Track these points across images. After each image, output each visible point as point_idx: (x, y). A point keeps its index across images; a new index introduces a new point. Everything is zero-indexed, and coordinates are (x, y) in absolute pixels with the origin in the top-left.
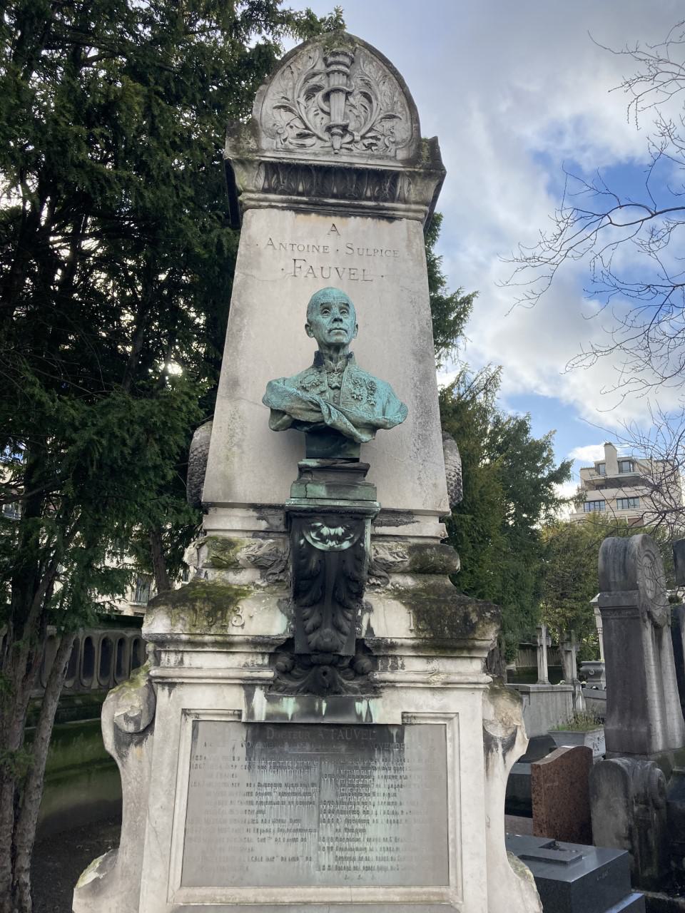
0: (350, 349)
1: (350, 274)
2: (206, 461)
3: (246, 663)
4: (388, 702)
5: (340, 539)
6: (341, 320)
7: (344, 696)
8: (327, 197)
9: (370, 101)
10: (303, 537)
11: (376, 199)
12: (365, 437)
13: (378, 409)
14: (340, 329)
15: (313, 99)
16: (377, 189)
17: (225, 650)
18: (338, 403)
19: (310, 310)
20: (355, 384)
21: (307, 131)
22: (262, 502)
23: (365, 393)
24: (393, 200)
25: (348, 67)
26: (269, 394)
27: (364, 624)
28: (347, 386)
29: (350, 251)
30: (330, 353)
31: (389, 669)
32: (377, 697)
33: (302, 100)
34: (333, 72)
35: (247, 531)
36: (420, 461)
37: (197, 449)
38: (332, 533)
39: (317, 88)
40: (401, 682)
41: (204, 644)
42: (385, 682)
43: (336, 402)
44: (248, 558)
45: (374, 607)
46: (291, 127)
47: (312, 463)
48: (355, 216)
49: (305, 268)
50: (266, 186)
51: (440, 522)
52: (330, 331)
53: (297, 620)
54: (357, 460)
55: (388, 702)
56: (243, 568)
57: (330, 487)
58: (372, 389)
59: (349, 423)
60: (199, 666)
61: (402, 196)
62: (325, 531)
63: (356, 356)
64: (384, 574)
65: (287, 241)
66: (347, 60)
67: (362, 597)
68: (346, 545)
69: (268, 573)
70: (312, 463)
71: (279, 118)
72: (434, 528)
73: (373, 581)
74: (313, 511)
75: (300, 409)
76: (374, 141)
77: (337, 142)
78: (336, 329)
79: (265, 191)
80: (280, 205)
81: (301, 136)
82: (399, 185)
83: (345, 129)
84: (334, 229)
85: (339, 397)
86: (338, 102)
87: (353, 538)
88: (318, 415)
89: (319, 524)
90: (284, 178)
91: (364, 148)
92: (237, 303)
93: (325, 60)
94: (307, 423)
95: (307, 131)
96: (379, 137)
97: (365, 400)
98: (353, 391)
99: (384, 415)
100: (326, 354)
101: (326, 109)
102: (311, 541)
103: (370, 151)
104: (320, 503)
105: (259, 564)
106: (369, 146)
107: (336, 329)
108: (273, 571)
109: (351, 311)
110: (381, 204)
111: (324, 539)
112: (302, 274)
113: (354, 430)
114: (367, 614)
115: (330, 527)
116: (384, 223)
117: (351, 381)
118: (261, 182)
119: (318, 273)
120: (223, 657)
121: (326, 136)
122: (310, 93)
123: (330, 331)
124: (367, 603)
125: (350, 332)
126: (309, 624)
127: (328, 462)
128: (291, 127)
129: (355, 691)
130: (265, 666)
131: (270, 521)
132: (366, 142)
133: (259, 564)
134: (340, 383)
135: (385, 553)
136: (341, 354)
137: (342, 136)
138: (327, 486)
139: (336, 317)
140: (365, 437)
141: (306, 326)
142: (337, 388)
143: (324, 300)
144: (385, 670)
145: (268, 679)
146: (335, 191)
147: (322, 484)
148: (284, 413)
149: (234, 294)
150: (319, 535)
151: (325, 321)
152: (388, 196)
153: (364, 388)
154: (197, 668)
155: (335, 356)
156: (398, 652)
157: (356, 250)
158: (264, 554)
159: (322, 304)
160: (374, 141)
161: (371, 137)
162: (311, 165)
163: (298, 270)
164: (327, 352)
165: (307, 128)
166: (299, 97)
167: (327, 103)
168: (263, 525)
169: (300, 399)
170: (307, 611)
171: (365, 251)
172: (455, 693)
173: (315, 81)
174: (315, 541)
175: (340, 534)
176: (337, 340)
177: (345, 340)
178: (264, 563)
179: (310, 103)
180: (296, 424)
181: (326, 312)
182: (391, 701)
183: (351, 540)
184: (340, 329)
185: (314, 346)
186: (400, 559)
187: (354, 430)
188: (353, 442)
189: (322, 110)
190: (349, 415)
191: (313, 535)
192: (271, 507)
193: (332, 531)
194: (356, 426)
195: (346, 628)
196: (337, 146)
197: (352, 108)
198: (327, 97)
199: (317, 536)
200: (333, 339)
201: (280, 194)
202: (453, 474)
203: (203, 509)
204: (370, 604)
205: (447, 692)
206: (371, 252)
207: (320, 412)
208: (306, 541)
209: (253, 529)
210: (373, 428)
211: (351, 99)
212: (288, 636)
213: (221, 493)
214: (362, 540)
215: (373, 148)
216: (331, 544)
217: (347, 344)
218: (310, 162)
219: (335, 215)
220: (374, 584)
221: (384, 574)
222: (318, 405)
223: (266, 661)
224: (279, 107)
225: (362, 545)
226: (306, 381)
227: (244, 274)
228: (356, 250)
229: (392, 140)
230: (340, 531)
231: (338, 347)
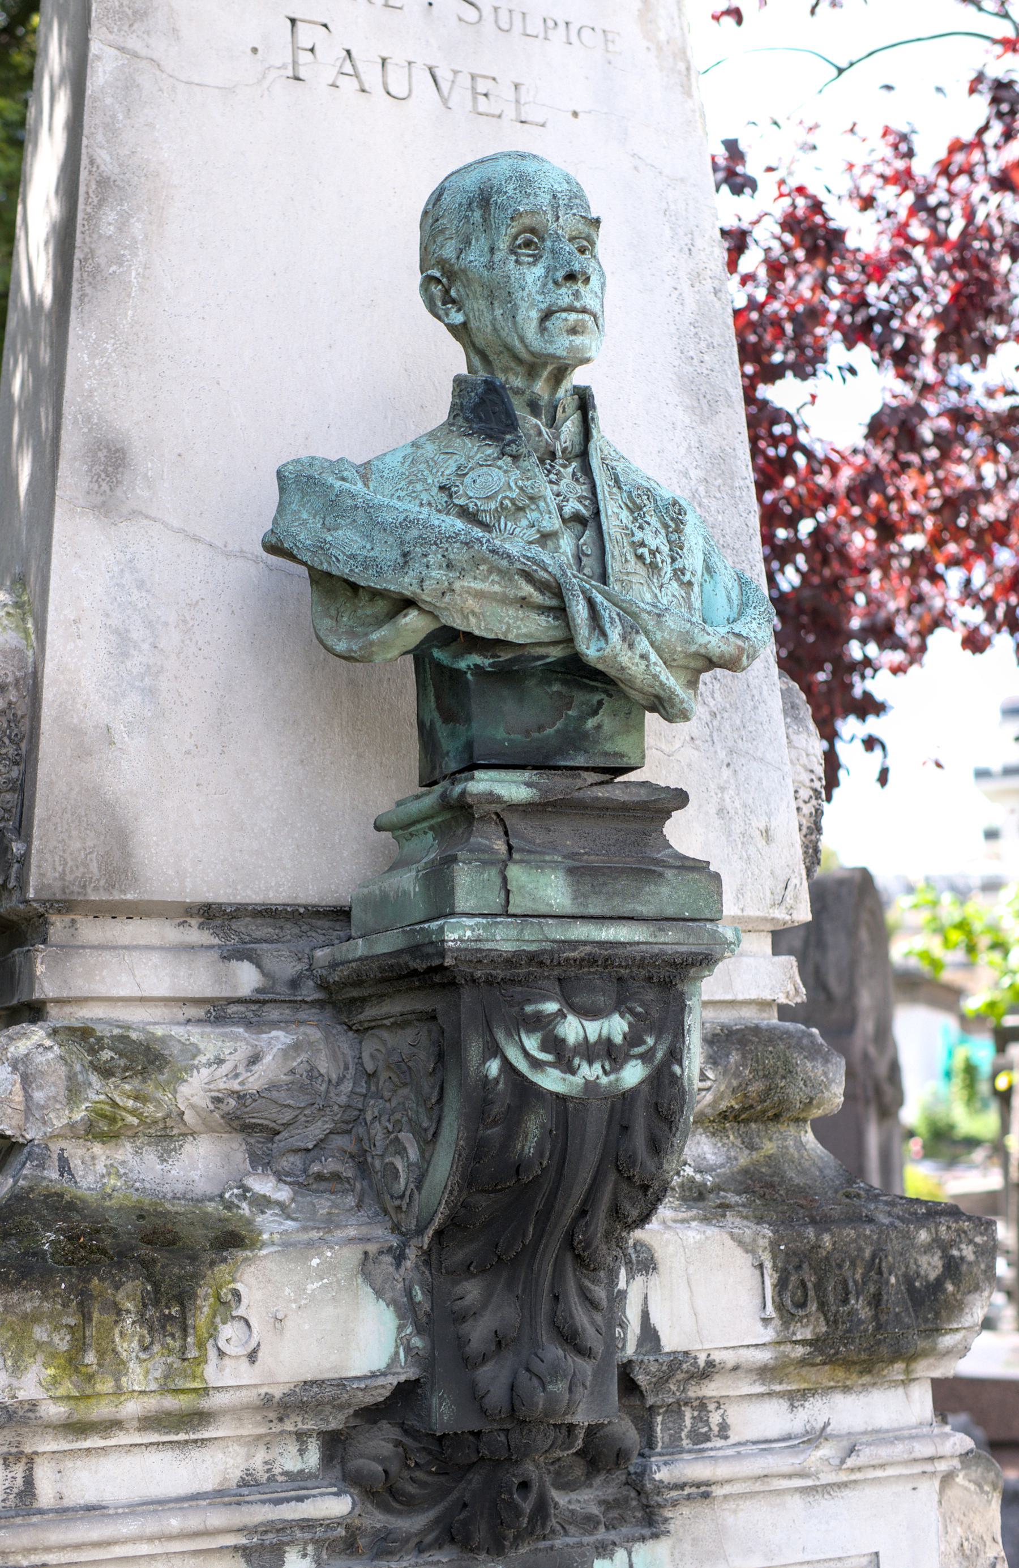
1: (475, 93)
3: (248, 1472)
4: (687, 1547)
5: (610, 1053)
7: (558, 1543)
10: (495, 1050)
17: (182, 1437)
22: (239, 899)
27: (632, 1314)
30: (509, 398)
31: (686, 1443)
32: (655, 1536)
35: (185, 1001)
36: (722, 754)
38: (592, 1038)
40: (728, 1481)
41: (114, 1425)
42: (682, 1486)
44: (217, 1100)
45: (659, 1255)
49: (330, 54)
51: (776, 952)
52: (547, 315)
53: (434, 1324)
55: (687, 1547)
57: (579, 873)
60: (91, 1497)
74: (534, 959)
87: (652, 1050)
89: (551, 1007)
92: (103, 156)
98: (639, 536)
102: (522, 1065)
104: (557, 932)
111: (563, 1055)
114: (639, 1279)
119: (372, 76)
120: (167, 1456)
126: (478, 1333)
127: (559, 784)
129: (589, 1523)
130: (311, 1476)
131: (269, 963)
138: (571, 871)
144: (674, 1448)
145: (339, 1521)
147: (555, 866)
150: (554, 1044)
154: (90, 1508)
156: (710, 1389)
158: (273, 1086)
163: (304, 57)
168: (246, 978)
170: (472, 1291)
172: (870, 1493)
175: (618, 1039)
178: (267, 1115)
182: (695, 1541)
183: (646, 1058)
191: (531, 1043)
192: (267, 913)
193: (594, 1029)
195: (592, 1338)
199: (544, 1048)
204: (649, 1249)
205: (847, 1493)
206: (535, 26)
208: (508, 1066)
209: (209, 993)
212: (407, 1373)
213: (94, 867)
214: (675, 1055)
216: (590, 1072)
223: (313, 1458)
225: (677, 1069)
227: (122, 49)
230: (616, 1027)
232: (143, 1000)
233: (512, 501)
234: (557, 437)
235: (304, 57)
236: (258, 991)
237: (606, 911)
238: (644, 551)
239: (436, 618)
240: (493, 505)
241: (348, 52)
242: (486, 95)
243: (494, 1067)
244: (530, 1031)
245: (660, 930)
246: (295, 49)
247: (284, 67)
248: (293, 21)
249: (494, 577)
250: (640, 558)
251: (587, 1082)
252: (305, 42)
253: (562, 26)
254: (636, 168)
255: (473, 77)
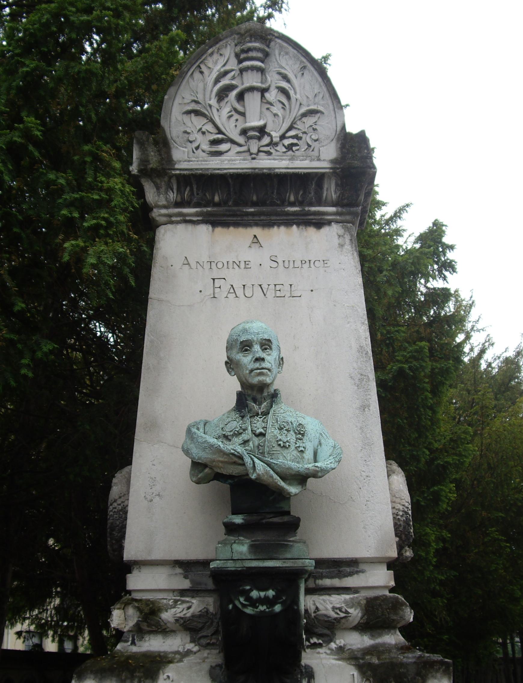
0: (274, 387)
1: (276, 291)
2: (126, 513)
5: (265, 601)
6: (263, 360)
8: (246, 205)
9: (288, 97)
10: (232, 602)
11: (301, 204)
12: (293, 490)
13: (308, 454)
14: (263, 368)
15: (226, 100)
16: (301, 193)
18: (263, 453)
19: (229, 348)
20: (281, 429)
21: (220, 136)
23: (292, 437)
24: (320, 203)
25: (262, 62)
26: (189, 442)
28: (272, 432)
29: (274, 265)
30: (254, 397)
33: (213, 102)
34: (247, 69)
35: (173, 591)
37: (115, 501)
39: (229, 88)
43: (261, 452)
46: (204, 133)
47: (238, 520)
48: (279, 225)
49: (226, 287)
50: (179, 199)
54: (288, 513)
56: (173, 631)
58: (301, 433)
59: (275, 476)
61: (329, 198)
62: (255, 594)
63: (283, 394)
64: (326, 631)
65: (205, 259)
66: (260, 55)
67: (300, 661)
68: (278, 608)
69: (200, 635)
70: (238, 520)
71: (189, 124)
72: (381, 578)
73: (314, 640)
75: (222, 462)
76: (295, 141)
77: (254, 146)
78: (258, 369)
79: (177, 205)
80: (195, 219)
81: (215, 142)
82: (326, 186)
83: (262, 131)
84: (255, 240)
85: (264, 446)
86: (253, 101)
88: (241, 468)
89: (248, 588)
90: (198, 189)
91: (285, 150)
93: (237, 56)
94: (231, 477)
95: (220, 136)
96: (300, 135)
97: (293, 448)
98: (280, 437)
99: (315, 461)
100: (249, 395)
101: (240, 108)
102: (240, 606)
103: (290, 152)
105: (189, 626)
106: (290, 147)
107: (258, 369)
108: (204, 634)
109: (274, 347)
110: (307, 209)
112: (221, 294)
113: (282, 484)
115: (260, 589)
116: (311, 230)
117: (277, 426)
118: (172, 196)
119: (240, 292)
121: (241, 140)
122: (222, 94)
123: (251, 371)
124: (307, 667)
125: (275, 370)
127: (255, 518)
128: (204, 133)
132: (287, 142)
133: (189, 626)
134: (265, 428)
135: (327, 605)
136: (265, 394)
137: (259, 139)
139: (257, 356)
140: (293, 490)
141: (226, 363)
142: (262, 435)
143: (243, 338)
146: (255, 198)
148: (205, 466)
149: (147, 327)
150: (249, 599)
151: (246, 360)
152: (314, 200)
153: (292, 432)
155: (258, 396)
157: (281, 263)
159: (241, 342)
160: (295, 141)
161: (292, 137)
162: (226, 174)
163: (217, 290)
164: (250, 392)
165: (220, 132)
166: (210, 99)
167: (242, 103)
169: (219, 451)
171: (292, 263)
173: (225, 81)
174: (244, 606)
176: (259, 381)
177: (268, 380)
179: (223, 104)
180: (219, 477)
181: (246, 350)
184: (263, 368)
185: (233, 385)
186: (342, 615)
187: (282, 484)
188: (282, 496)
189: (236, 110)
190: (275, 467)
191: (242, 599)
193: (262, 594)
194: (283, 478)
196: (254, 150)
197: (269, 106)
198: (240, 97)
199: (245, 600)
200: (255, 380)
201: (195, 206)
202: (401, 513)
203: (128, 567)
207: (244, 465)
208: (235, 606)
210: (301, 479)
211: (267, 95)
215: (294, 148)
216: (262, 608)
217: (272, 383)
218: (225, 171)
219: (257, 225)
220: (315, 643)
221: (326, 631)
222: (241, 458)
224: (189, 112)
225: (296, 607)
226: (228, 428)
228: (281, 263)
229: (314, 137)
230: (271, 593)
231: (262, 387)
232: (160, 591)
233: (238, 431)
234: (260, 408)
235: (217, 290)
236: (190, 587)
237: (264, 557)
238: (281, 443)
239: (213, 469)
240: (232, 433)
241: (232, 285)
242: (280, 290)
243: (231, 606)
244: (242, 596)
245: (284, 562)
246: (214, 288)
247: (210, 295)
248: (214, 279)
249: (225, 456)
250: (280, 445)
251: (261, 611)
252: (217, 285)
253: (308, 262)
254: (335, 305)
255: (275, 285)
